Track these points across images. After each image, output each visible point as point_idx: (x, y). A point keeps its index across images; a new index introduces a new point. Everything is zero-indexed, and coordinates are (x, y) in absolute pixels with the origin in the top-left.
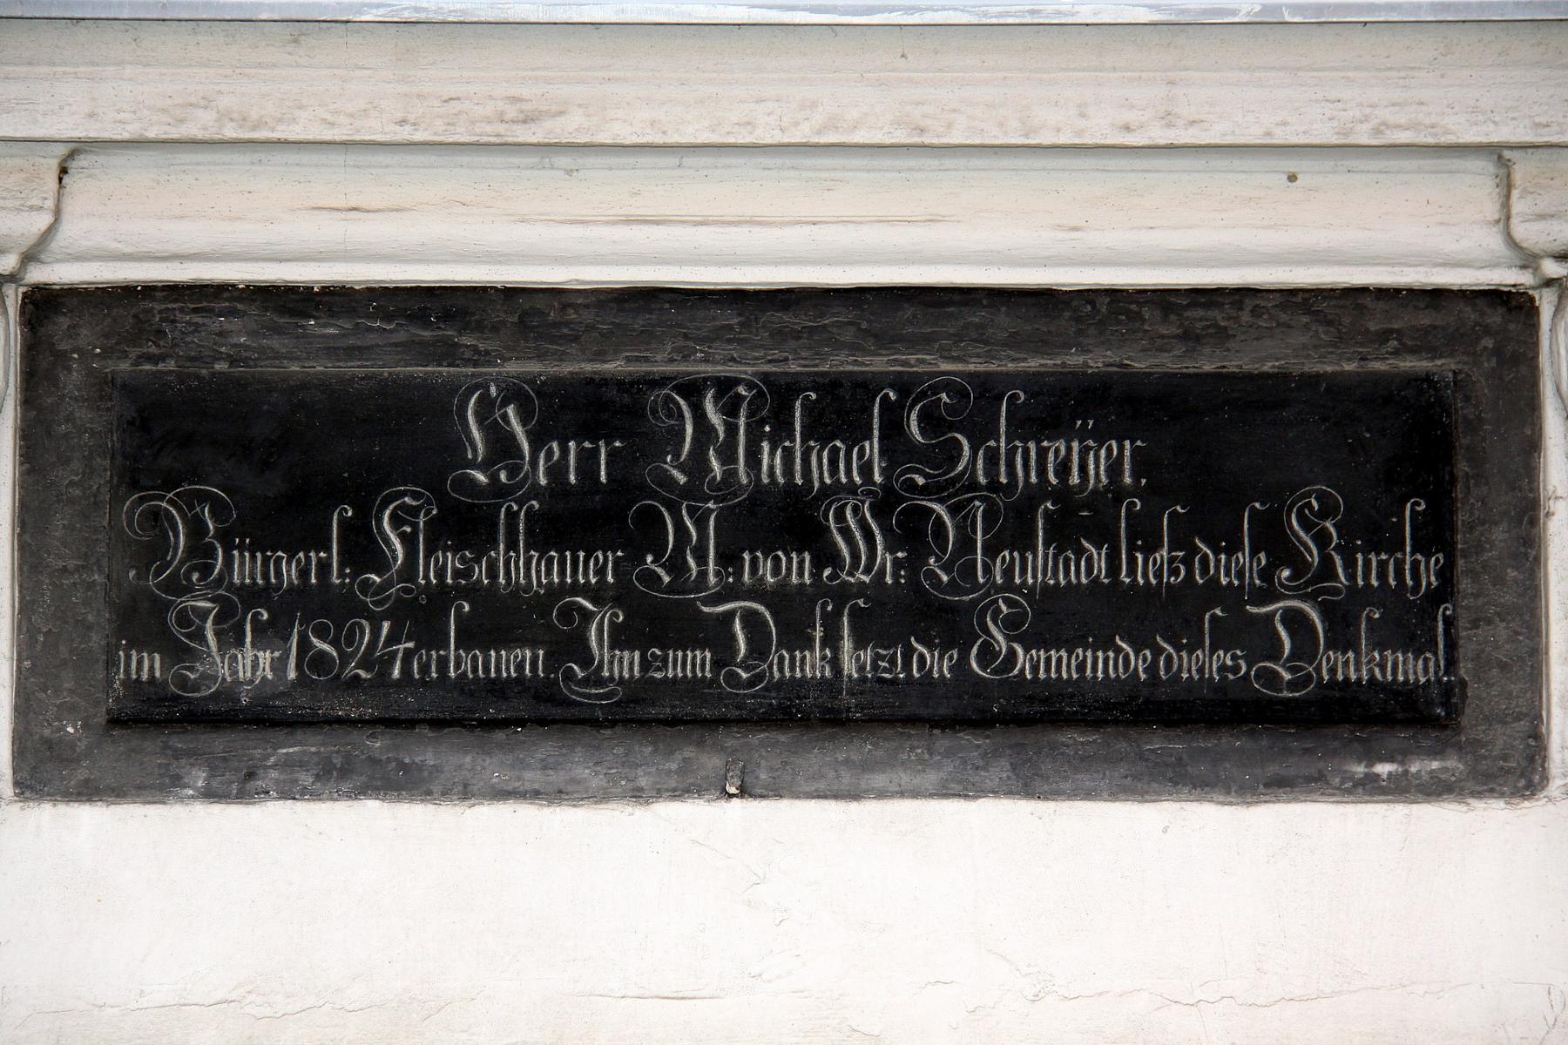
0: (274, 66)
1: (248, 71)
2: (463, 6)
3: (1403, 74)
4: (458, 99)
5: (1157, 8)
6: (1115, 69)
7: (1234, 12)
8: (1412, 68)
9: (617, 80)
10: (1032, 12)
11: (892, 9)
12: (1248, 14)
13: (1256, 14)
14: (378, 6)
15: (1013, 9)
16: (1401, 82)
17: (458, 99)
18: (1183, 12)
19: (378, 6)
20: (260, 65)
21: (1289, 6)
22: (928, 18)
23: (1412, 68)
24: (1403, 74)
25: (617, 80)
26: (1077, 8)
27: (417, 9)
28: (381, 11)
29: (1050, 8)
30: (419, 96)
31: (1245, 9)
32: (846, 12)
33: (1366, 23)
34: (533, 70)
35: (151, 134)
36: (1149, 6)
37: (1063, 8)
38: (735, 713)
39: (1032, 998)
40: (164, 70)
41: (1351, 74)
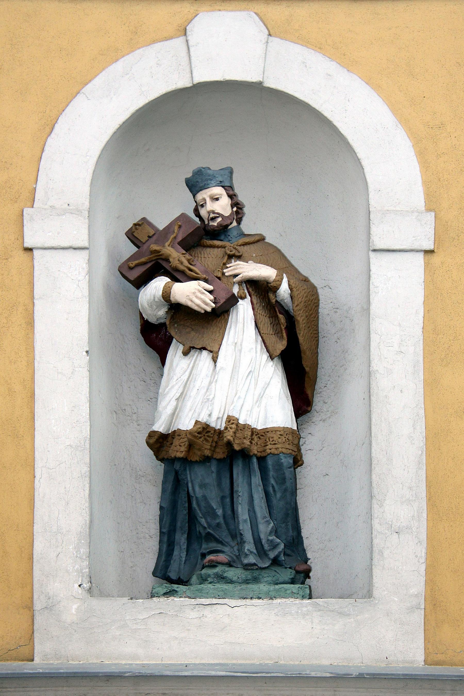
0: (102, 686)
1: (95, 688)
2: (152, 672)
3: (395, 690)
4: (149, 694)
5: (332, 673)
6: (320, 687)
7: (352, 675)
8: (397, 689)
9: (191, 689)
10: (299, 674)
11: (263, 673)
12: (355, 675)
13: (357, 675)
14: (130, 672)
15: (294, 673)
16: (395, 692)
17: (149, 694)
18: (338, 674)
19: (130, 672)
20: (98, 686)
21: (366, 674)
22: (272, 675)
23: (397, 689)
24: (395, 690)
25: (191, 689)
26: (311, 673)
27: (140, 673)
28: (130, 673)
29: (304, 673)
30: (139, 693)
31: (354, 674)
32: (251, 673)
33: (385, 678)
34: (169, 687)
35: (192, 58)
36: (329, 673)
37: (307, 673)
38: (267, 385)
39: (338, 310)
40: (74, 688)
41: (382, 690)
